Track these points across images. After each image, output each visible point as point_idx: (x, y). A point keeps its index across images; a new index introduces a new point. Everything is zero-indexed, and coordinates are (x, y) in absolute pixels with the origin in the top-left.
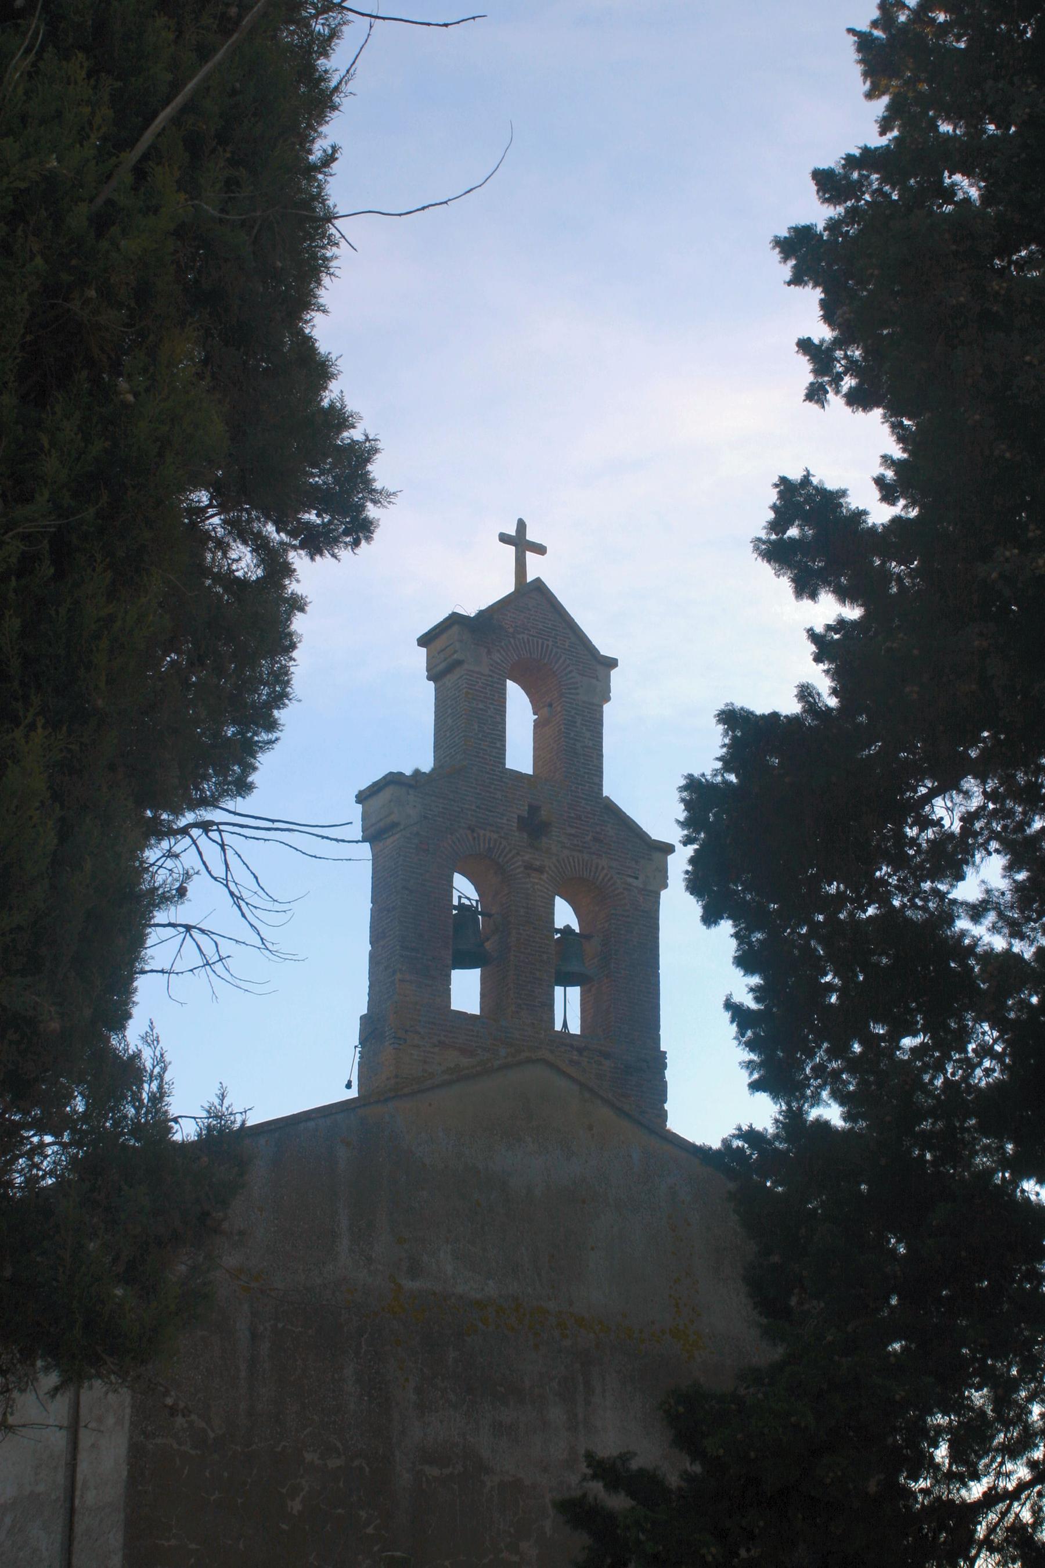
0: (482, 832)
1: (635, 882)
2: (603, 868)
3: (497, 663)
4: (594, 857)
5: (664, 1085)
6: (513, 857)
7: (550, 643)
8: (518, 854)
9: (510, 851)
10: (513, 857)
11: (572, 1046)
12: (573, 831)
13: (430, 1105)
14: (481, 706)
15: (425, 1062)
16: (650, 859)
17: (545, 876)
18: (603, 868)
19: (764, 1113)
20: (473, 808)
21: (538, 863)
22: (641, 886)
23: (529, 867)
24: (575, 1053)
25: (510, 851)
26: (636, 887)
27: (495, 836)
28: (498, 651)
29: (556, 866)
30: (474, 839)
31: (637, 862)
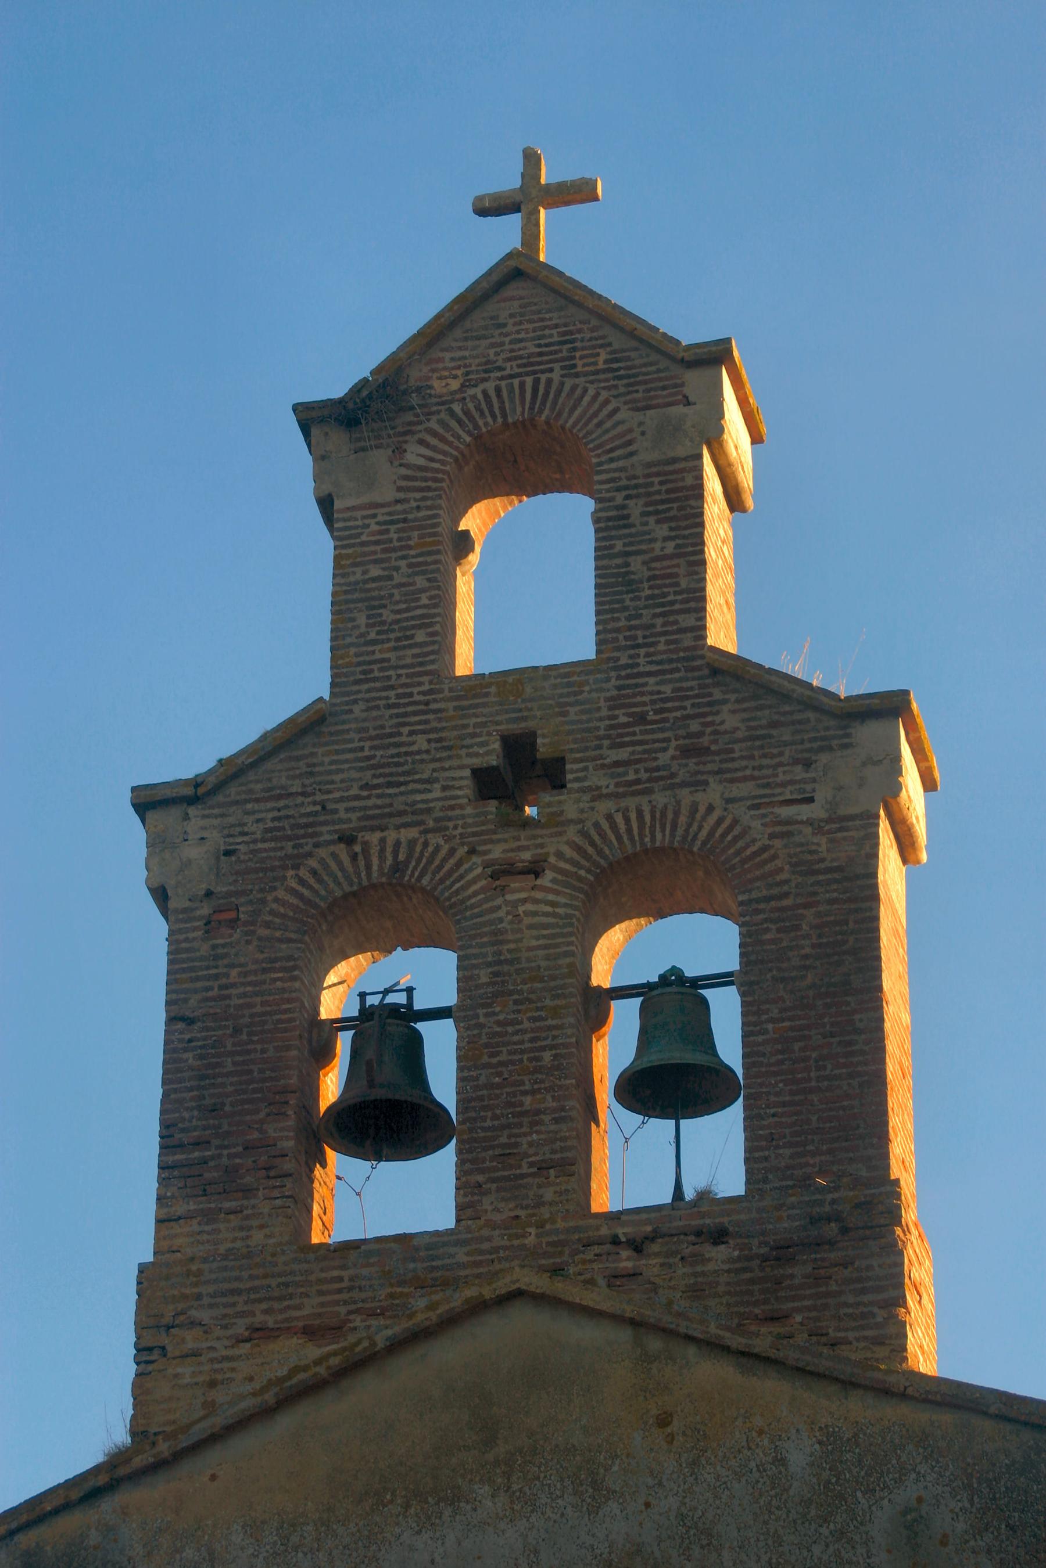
0: (374, 838)
1: (804, 812)
2: (710, 809)
3: (420, 468)
4: (685, 791)
5: (66, 1481)
6: (459, 864)
7: (556, 376)
8: (472, 852)
9: (452, 852)
10: (459, 864)
11: (615, 1241)
12: (623, 754)
13: (213, 1477)
14: (375, 571)
15: (212, 1384)
16: (846, 746)
17: (547, 879)
18: (710, 809)
19: (734, 1114)
20: (354, 791)
21: (527, 856)
22: (823, 815)
23: (502, 872)
24: (625, 1253)
25: (452, 852)
26: (810, 822)
27: (413, 833)
28: (421, 442)
29: (579, 849)
30: (354, 857)
31: (808, 764)
